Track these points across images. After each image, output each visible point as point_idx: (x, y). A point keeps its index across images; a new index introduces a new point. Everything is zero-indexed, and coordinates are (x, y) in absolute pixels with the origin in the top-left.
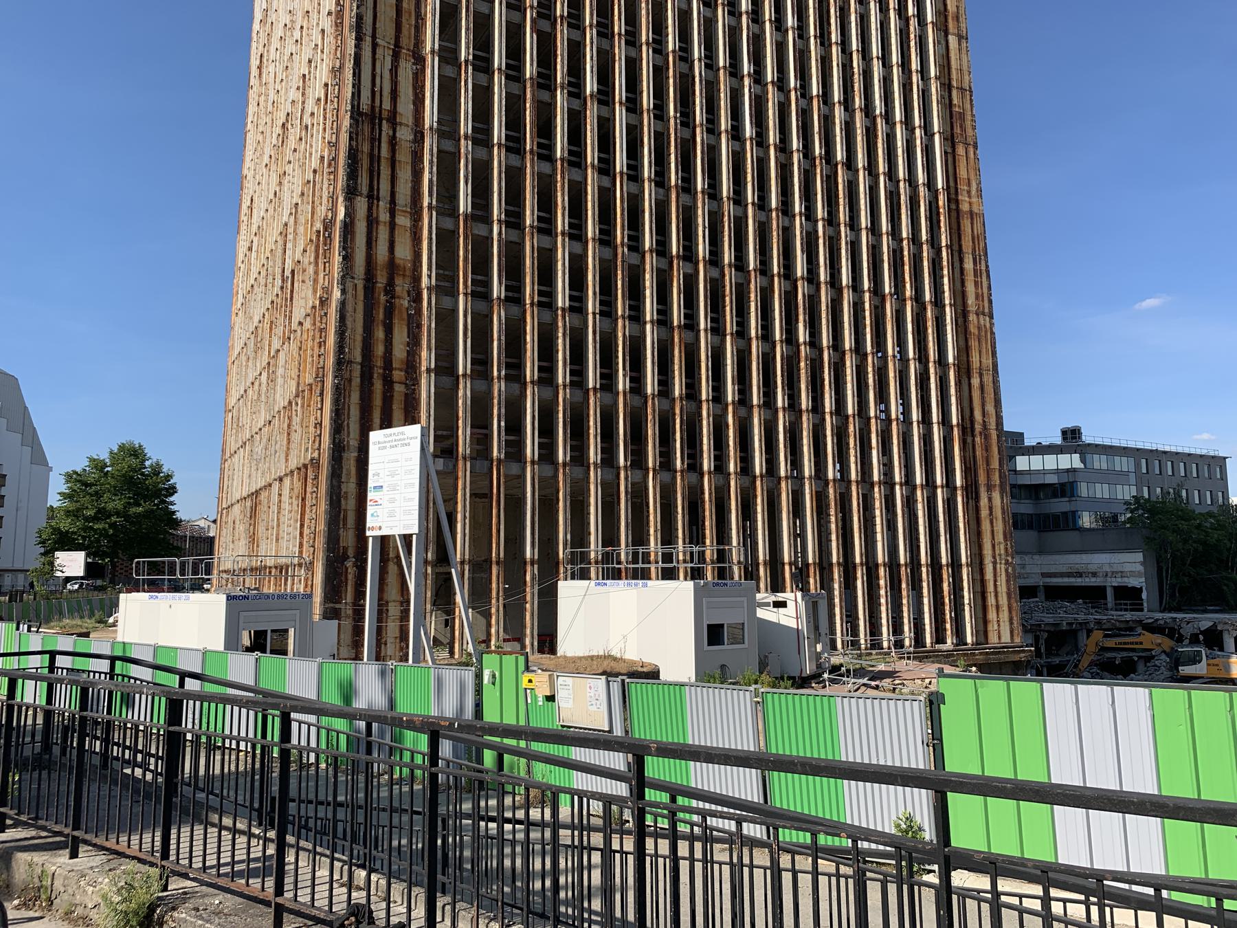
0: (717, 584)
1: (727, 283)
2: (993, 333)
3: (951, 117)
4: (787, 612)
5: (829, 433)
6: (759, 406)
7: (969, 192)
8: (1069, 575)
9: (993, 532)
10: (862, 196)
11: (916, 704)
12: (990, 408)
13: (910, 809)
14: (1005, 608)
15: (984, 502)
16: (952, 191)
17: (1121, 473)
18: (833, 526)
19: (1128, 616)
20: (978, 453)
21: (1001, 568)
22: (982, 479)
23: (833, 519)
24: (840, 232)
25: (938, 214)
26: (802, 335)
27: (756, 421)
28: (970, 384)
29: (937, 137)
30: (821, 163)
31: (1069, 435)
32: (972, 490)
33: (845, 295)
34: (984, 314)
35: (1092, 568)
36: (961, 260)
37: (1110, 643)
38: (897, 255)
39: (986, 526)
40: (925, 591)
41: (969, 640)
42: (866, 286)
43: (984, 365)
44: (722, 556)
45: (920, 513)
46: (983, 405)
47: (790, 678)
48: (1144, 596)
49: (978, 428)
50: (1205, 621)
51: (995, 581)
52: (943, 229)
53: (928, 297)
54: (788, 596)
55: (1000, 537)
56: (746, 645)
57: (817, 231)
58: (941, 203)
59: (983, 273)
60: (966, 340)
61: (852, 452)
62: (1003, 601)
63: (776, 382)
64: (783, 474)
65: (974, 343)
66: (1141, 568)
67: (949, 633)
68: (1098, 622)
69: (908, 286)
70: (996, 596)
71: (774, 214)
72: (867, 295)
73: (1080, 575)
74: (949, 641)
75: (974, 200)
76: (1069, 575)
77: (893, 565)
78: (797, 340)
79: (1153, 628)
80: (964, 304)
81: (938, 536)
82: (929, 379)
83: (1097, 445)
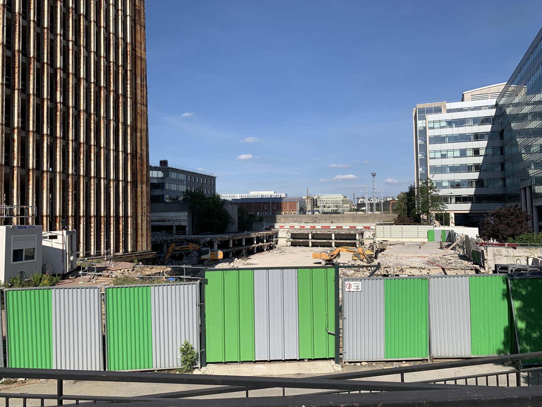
0: (20, 227)
1: (17, 61)
2: (147, 114)
3: (135, 11)
4: (58, 241)
5: (70, 150)
6: (33, 132)
7: (141, 48)
8: (159, 221)
9: (142, 202)
10: (92, 35)
11: (194, 286)
12: (144, 147)
13: (187, 339)
14: (145, 236)
15: (139, 189)
16: (134, 45)
17: (181, 181)
18: (70, 197)
19: (182, 237)
20: (138, 167)
21: (145, 218)
22: (139, 179)
23: (70, 194)
24: (80, 50)
25: (127, 54)
26: (59, 98)
27: (31, 140)
28: (136, 135)
29: (128, 18)
30: (72, 12)
31: (163, 164)
32: (134, 183)
33: (82, 83)
34: (144, 105)
35: (169, 218)
36: (136, 78)
37: (178, 248)
38: (107, 68)
39: (139, 199)
40: (112, 229)
41: (129, 250)
42: (92, 81)
43: (143, 128)
44: (23, 212)
45: (112, 193)
46: (141, 146)
47: (59, 275)
48: (187, 229)
49: (139, 155)
50: (208, 238)
51: (142, 224)
52: (129, 62)
53: (120, 92)
54: (58, 233)
55: (145, 205)
56: (35, 260)
57: (68, 47)
58: (128, 49)
59: (144, 87)
60: (136, 115)
61: (82, 161)
62: (145, 232)
63: (43, 121)
64: (45, 169)
65: (139, 117)
66: (186, 218)
67: (121, 247)
68: (171, 240)
69: (112, 85)
70: (142, 230)
71: (46, 31)
72: (93, 85)
73: (164, 221)
74: (121, 251)
75: (143, 52)
76: (159, 221)
77: (98, 216)
78: (56, 100)
79: (192, 241)
80: (136, 99)
81: (119, 203)
82: (119, 130)
83: (173, 169)
